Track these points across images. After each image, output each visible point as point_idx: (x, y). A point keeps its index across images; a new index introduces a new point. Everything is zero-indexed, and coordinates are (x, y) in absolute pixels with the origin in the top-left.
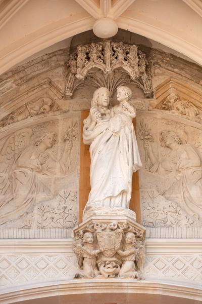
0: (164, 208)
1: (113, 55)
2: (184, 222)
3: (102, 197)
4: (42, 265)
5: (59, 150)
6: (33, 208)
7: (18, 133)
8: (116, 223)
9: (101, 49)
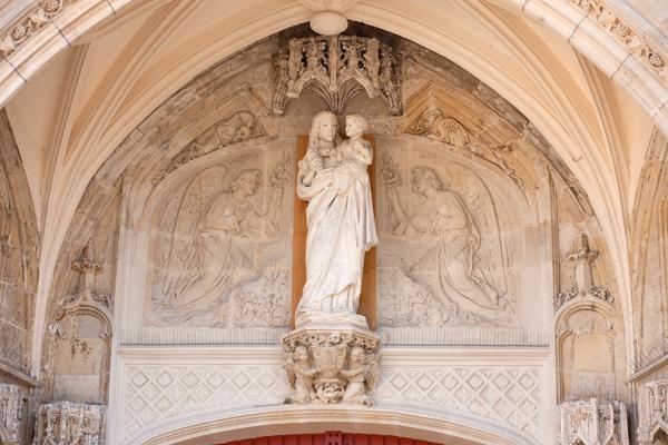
1: (343, 57)
2: (436, 318)
3: (320, 297)
4: (241, 381)
6: (228, 296)
7: (204, 174)
8: (338, 335)
9: (324, 48)
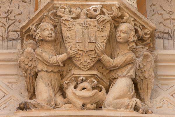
8: (99, 7)
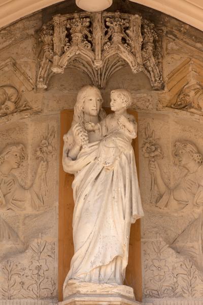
0: (174, 268)
1: (106, 33)
5: (29, 170)
9: (88, 24)
